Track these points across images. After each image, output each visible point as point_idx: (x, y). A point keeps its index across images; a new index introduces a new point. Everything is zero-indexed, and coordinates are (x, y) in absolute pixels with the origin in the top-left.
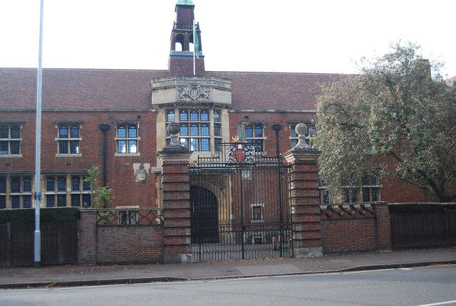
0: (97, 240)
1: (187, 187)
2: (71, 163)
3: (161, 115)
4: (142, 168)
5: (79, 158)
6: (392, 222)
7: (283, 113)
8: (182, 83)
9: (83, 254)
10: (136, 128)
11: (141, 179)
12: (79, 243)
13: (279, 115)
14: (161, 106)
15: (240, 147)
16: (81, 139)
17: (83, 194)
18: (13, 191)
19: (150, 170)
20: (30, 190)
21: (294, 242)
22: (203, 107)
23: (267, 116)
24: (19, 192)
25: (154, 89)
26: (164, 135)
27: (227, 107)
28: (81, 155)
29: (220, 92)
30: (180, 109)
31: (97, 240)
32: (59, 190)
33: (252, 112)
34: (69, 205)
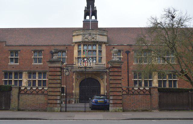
3: (76, 48)
7: (130, 45)
8: (85, 33)
13: (128, 47)
14: (76, 43)
16: (42, 57)
17: (43, 80)
18: (15, 78)
20: (22, 78)
22: (94, 43)
23: (123, 47)
27: (105, 43)
29: (101, 36)
32: (33, 78)
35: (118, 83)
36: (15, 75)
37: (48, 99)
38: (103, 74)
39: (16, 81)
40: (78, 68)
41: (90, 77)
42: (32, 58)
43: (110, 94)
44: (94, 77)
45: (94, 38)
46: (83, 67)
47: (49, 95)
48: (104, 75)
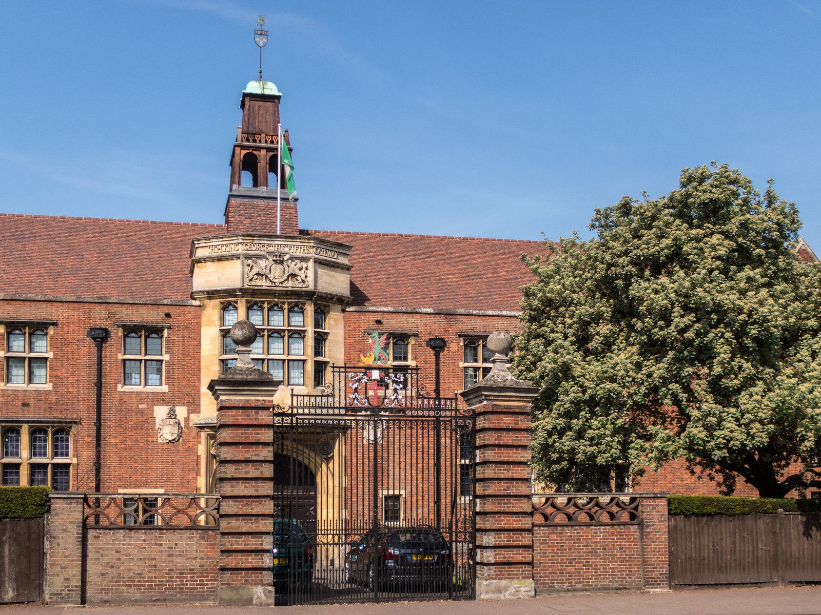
1: (267, 453)
2: (32, 401)
4: (172, 414)
5: (47, 392)
6: (672, 532)
11: (170, 438)
12: (48, 560)
13: (441, 318)
14: (211, 294)
15: (376, 375)
19: (187, 420)
21: (478, 567)
25: (199, 261)
26: (217, 352)
28: (49, 387)
30: (248, 302)
34: (24, 482)
35: (515, 476)
36: (33, 440)
37: (222, 552)
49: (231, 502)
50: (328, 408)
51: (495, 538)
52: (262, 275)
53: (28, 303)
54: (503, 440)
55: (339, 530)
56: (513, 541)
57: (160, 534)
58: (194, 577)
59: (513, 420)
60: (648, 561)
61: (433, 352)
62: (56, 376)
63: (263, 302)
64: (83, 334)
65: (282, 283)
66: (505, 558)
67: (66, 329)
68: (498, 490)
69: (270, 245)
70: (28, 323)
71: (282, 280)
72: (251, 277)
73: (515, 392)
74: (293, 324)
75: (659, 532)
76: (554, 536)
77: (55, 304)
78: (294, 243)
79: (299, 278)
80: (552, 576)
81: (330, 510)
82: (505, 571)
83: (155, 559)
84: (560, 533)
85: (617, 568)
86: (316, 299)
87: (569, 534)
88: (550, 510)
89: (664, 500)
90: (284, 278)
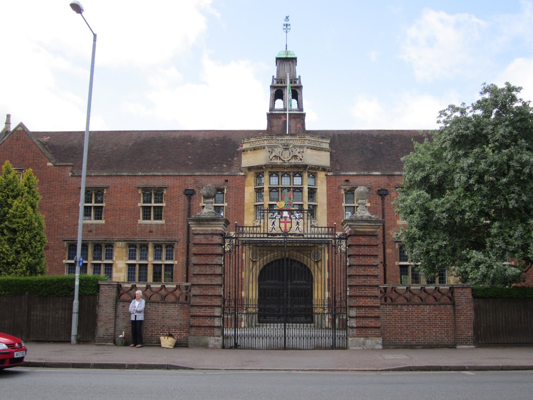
0: (116, 316)
2: (154, 230)
6: (477, 310)
8: (273, 143)
9: (101, 331)
10: (223, 193)
14: (250, 169)
15: (286, 214)
18: (94, 259)
20: (111, 258)
24: (100, 259)
27: (324, 169)
29: (315, 152)
30: (270, 172)
31: (116, 316)
32: (141, 259)
33: (353, 175)
37: (192, 316)
38: (321, 250)
39: (97, 267)
40: (266, 236)
41: (287, 256)
42: (139, 208)
43: (350, 302)
44: (296, 256)
45: (296, 156)
46: (280, 234)
47: (192, 306)
48: (323, 251)
49: (196, 288)
50: (257, 234)
51: (356, 311)
52: (278, 157)
53: (153, 177)
54: (361, 252)
55: (318, 305)
56: (368, 314)
57: (158, 305)
58: (176, 330)
59: (368, 240)
60: (459, 328)
61: (380, 198)
62: (167, 216)
63: (278, 172)
64: (181, 193)
65: (288, 161)
66: (363, 324)
67: (172, 191)
68: (358, 282)
69: (282, 140)
70: (153, 188)
71: (288, 159)
72: (271, 158)
73: (369, 223)
74: (295, 184)
75: (466, 309)
76: (396, 311)
77: (167, 177)
78: (296, 138)
79: (298, 158)
80: (395, 336)
81: (320, 292)
82: (363, 332)
83: (155, 320)
84: (400, 309)
85: (438, 332)
86: (309, 169)
87: (406, 310)
88: (423, 295)
89: (469, 289)
90: (290, 158)
